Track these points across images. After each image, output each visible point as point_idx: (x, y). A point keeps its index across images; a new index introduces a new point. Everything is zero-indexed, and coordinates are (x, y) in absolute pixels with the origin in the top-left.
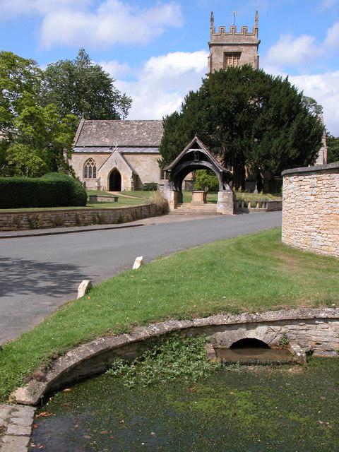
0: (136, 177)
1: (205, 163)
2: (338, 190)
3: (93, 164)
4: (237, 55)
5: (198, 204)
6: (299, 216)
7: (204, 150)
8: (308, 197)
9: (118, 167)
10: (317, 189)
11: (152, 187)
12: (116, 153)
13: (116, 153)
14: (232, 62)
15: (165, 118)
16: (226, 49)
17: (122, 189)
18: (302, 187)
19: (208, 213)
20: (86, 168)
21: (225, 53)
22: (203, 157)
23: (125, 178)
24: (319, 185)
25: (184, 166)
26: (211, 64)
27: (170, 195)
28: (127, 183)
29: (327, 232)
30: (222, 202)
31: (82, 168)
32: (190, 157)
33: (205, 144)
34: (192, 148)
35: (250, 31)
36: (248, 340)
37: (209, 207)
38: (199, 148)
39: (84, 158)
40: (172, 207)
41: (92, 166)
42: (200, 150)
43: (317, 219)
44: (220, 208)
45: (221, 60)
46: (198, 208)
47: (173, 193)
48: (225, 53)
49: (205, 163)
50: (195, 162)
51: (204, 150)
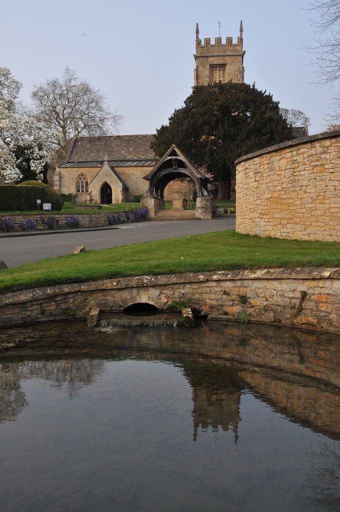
0: (126, 189)
1: (183, 171)
2: (339, 218)
3: (84, 178)
4: (223, 66)
5: (178, 210)
6: (246, 204)
7: (181, 157)
8: (252, 184)
9: (108, 182)
10: (259, 175)
11: (138, 199)
12: (106, 167)
13: (106, 167)
14: (218, 77)
15: (100, 93)
16: (211, 60)
17: (113, 202)
18: (248, 175)
19: (182, 216)
20: (77, 183)
21: (210, 65)
22: (181, 164)
23: (116, 191)
24: (261, 170)
25: (163, 173)
26: (197, 77)
27: (150, 203)
28: (117, 194)
29: (268, 217)
30: (200, 208)
31: (75, 183)
32: (168, 164)
33: (182, 151)
34: (169, 156)
35: (235, 42)
36: (140, 304)
37: (188, 213)
38: (176, 155)
39: (75, 172)
40: (152, 214)
41: (84, 181)
42: (178, 158)
43: (260, 205)
44: (198, 213)
45: (207, 73)
46: (177, 214)
47: (153, 201)
48: (210, 65)
49: (183, 171)
50: (174, 169)
51: (181, 157)
